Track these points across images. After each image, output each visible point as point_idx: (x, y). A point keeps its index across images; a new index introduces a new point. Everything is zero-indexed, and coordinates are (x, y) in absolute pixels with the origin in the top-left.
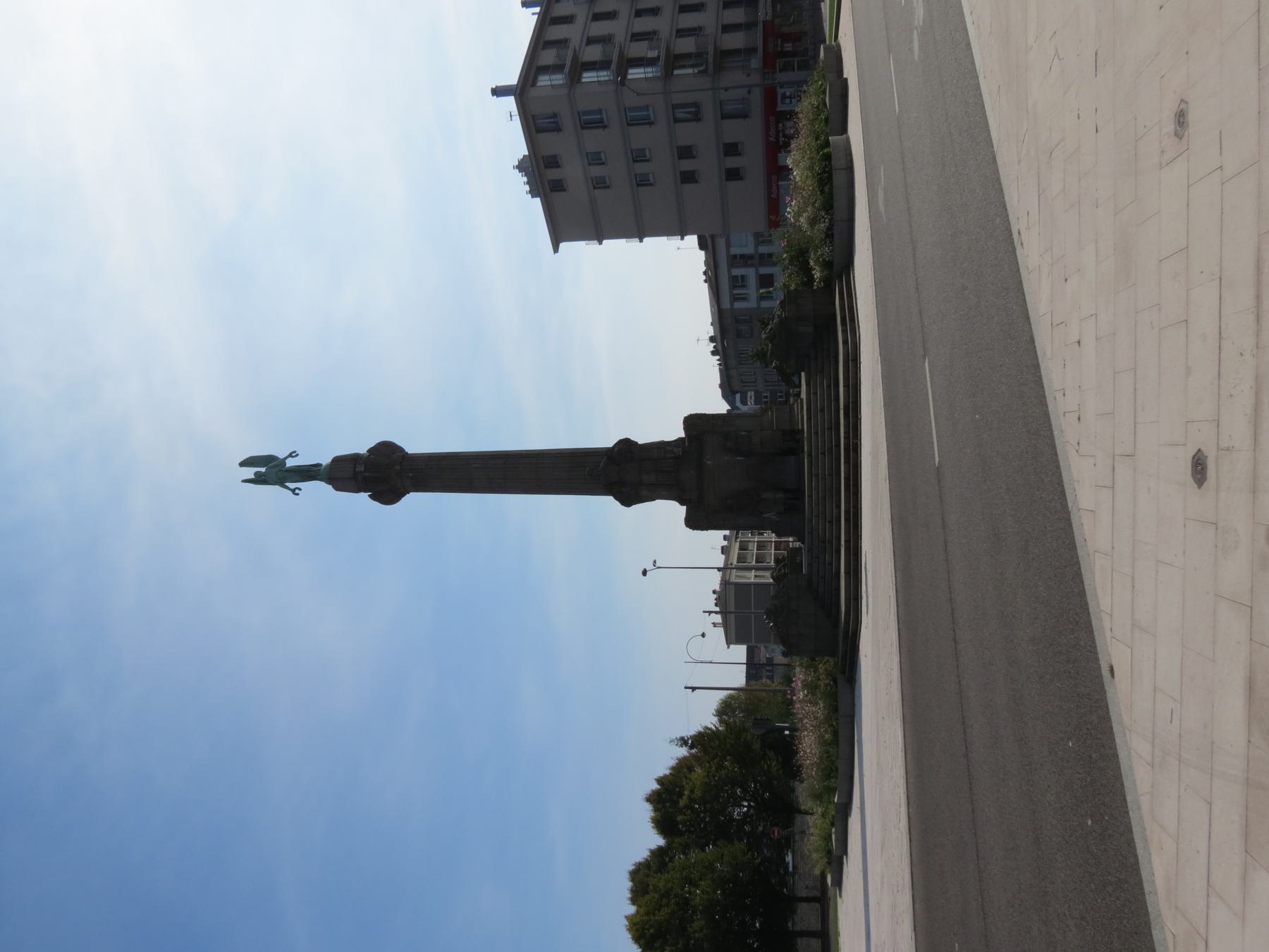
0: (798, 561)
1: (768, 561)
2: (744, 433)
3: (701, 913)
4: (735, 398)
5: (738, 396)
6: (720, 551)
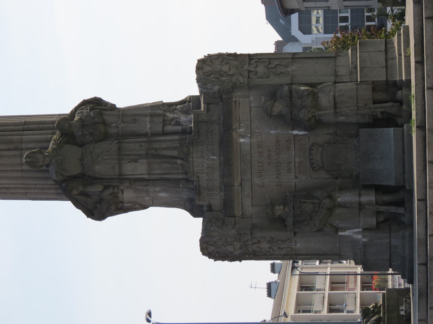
0: (402, 313)
1: (349, 308)
2: (302, 88)
3: (361, 33)
4: (289, 22)
5: (295, 17)
6: (265, 292)
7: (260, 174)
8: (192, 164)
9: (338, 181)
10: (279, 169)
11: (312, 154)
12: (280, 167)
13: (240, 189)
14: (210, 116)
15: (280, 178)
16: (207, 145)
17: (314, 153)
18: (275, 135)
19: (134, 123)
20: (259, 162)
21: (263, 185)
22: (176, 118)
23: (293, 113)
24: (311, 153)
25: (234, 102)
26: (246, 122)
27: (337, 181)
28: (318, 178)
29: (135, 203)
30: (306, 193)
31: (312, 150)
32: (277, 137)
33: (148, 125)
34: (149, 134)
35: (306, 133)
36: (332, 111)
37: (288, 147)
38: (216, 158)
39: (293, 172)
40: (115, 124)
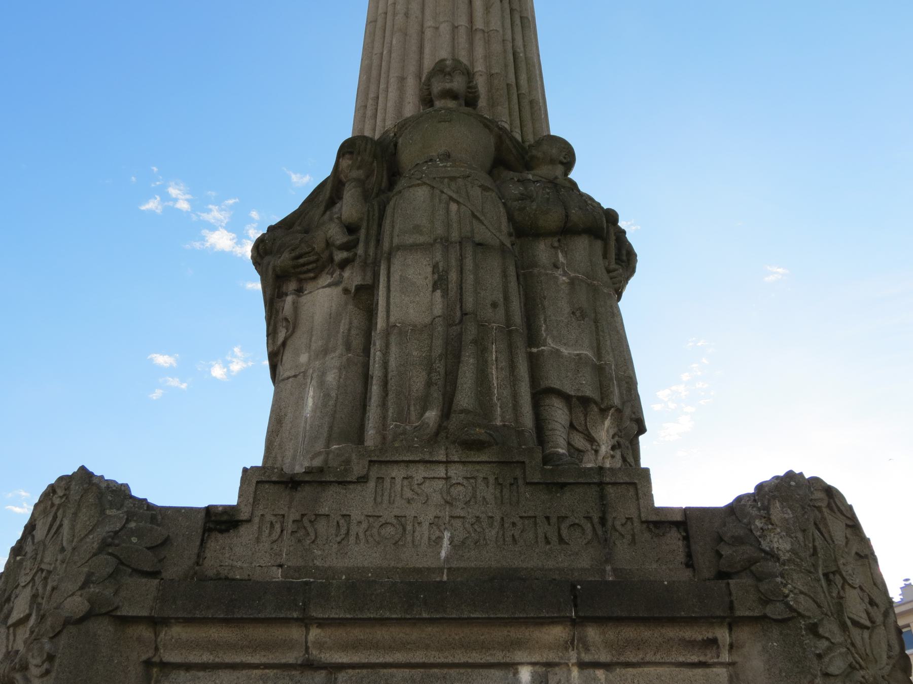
8: (418, 459)
13: (291, 657)
14: (633, 536)
16: (502, 519)
19: (573, 313)
22: (596, 451)
25: (710, 636)
29: (293, 325)
33: (566, 349)
34: (534, 350)
38: (443, 554)
40: (565, 262)
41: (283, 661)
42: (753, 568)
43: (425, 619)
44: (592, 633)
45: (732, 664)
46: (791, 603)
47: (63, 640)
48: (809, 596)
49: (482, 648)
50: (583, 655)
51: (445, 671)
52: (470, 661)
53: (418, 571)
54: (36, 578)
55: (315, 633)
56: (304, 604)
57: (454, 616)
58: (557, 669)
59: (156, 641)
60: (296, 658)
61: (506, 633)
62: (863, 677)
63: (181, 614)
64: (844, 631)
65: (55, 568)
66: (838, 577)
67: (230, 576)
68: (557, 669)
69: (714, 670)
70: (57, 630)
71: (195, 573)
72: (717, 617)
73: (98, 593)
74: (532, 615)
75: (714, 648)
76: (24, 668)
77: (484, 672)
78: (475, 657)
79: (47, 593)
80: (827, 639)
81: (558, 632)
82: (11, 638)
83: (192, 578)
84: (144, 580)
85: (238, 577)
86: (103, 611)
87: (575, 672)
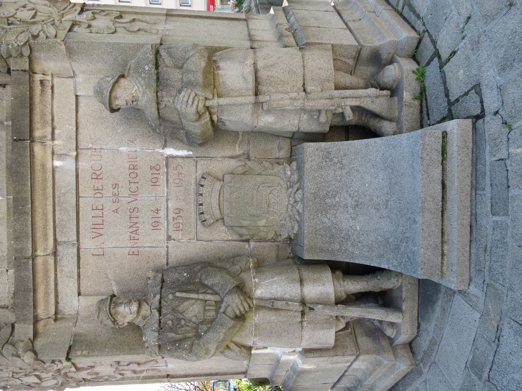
7: (96, 231)
9: (249, 245)
10: (136, 223)
11: (201, 195)
12: (138, 217)
13: (51, 260)
15: (138, 239)
17: (205, 192)
18: (128, 155)
20: (96, 208)
21: (103, 254)
23: (161, 101)
24: (200, 192)
25: (39, 83)
26: (67, 126)
27: (247, 246)
28: (211, 241)
30: (187, 275)
31: (202, 186)
32: (132, 160)
35: (191, 153)
36: (251, 99)
37: (154, 179)
39: (163, 229)
41: (53, 264)
42: (5, 57)
43: (32, 206)
44: (37, 134)
45: (52, 75)
46: (22, 44)
47: (45, 359)
48: (19, 35)
49: (45, 181)
50: (48, 138)
51: (56, 197)
52: (52, 186)
53: (8, 209)
54: (17, 377)
55: (39, 253)
56: (25, 259)
57: (30, 194)
58: (55, 150)
59: (45, 319)
60: (52, 259)
61: (38, 171)
62: (58, 21)
63: (32, 311)
64: (37, 23)
65: (11, 371)
66: (10, 19)
67: (13, 292)
68: (55, 150)
69: (55, 83)
70: (41, 362)
71: (12, 308)
72: (30, 78)
73: (22, 349)
74: (29, 159)
75: (45, 82)
76: (59, 370)
77: (56, 181)
78: (50, 184)
79: (23, 371)
80: (39, 32)
81: (37, 148)
82: (46, 379)
83: (14, 309)
84: (16, 330)
85: (13, 289)
86: (31, 345)
87: (56, 142)
